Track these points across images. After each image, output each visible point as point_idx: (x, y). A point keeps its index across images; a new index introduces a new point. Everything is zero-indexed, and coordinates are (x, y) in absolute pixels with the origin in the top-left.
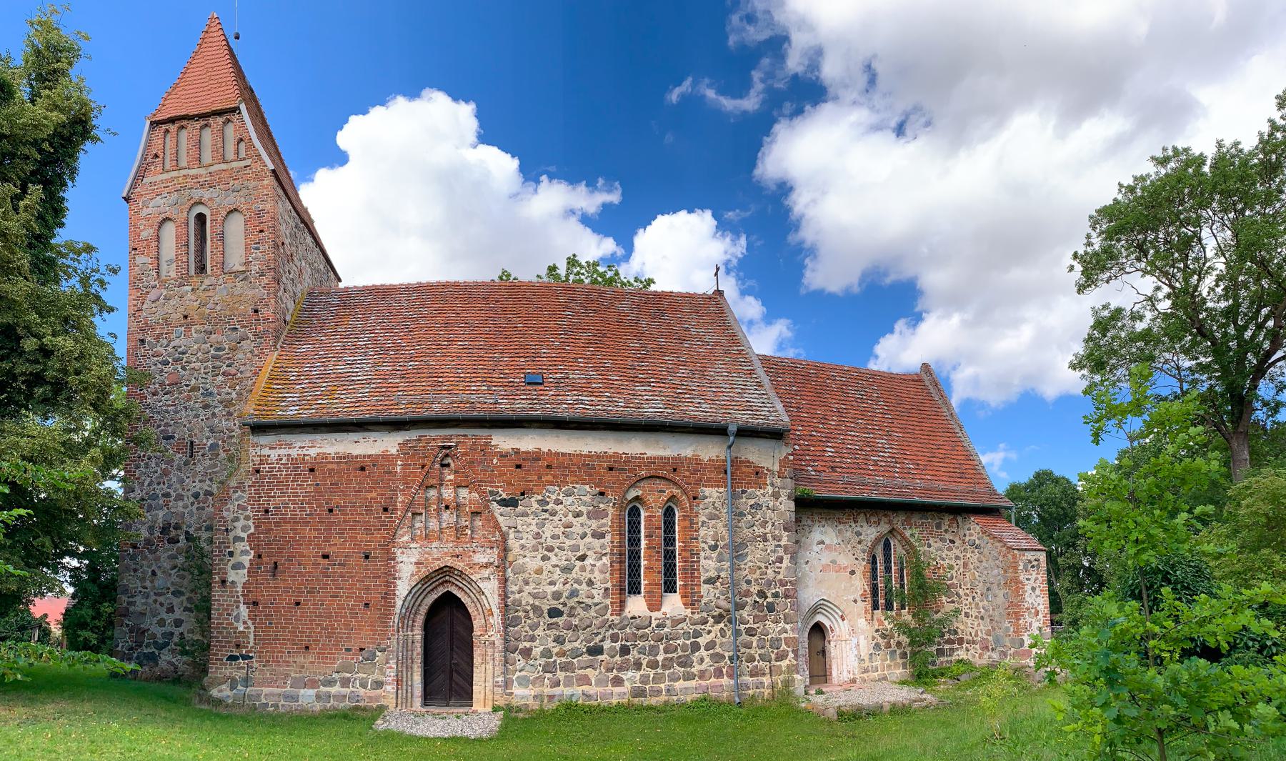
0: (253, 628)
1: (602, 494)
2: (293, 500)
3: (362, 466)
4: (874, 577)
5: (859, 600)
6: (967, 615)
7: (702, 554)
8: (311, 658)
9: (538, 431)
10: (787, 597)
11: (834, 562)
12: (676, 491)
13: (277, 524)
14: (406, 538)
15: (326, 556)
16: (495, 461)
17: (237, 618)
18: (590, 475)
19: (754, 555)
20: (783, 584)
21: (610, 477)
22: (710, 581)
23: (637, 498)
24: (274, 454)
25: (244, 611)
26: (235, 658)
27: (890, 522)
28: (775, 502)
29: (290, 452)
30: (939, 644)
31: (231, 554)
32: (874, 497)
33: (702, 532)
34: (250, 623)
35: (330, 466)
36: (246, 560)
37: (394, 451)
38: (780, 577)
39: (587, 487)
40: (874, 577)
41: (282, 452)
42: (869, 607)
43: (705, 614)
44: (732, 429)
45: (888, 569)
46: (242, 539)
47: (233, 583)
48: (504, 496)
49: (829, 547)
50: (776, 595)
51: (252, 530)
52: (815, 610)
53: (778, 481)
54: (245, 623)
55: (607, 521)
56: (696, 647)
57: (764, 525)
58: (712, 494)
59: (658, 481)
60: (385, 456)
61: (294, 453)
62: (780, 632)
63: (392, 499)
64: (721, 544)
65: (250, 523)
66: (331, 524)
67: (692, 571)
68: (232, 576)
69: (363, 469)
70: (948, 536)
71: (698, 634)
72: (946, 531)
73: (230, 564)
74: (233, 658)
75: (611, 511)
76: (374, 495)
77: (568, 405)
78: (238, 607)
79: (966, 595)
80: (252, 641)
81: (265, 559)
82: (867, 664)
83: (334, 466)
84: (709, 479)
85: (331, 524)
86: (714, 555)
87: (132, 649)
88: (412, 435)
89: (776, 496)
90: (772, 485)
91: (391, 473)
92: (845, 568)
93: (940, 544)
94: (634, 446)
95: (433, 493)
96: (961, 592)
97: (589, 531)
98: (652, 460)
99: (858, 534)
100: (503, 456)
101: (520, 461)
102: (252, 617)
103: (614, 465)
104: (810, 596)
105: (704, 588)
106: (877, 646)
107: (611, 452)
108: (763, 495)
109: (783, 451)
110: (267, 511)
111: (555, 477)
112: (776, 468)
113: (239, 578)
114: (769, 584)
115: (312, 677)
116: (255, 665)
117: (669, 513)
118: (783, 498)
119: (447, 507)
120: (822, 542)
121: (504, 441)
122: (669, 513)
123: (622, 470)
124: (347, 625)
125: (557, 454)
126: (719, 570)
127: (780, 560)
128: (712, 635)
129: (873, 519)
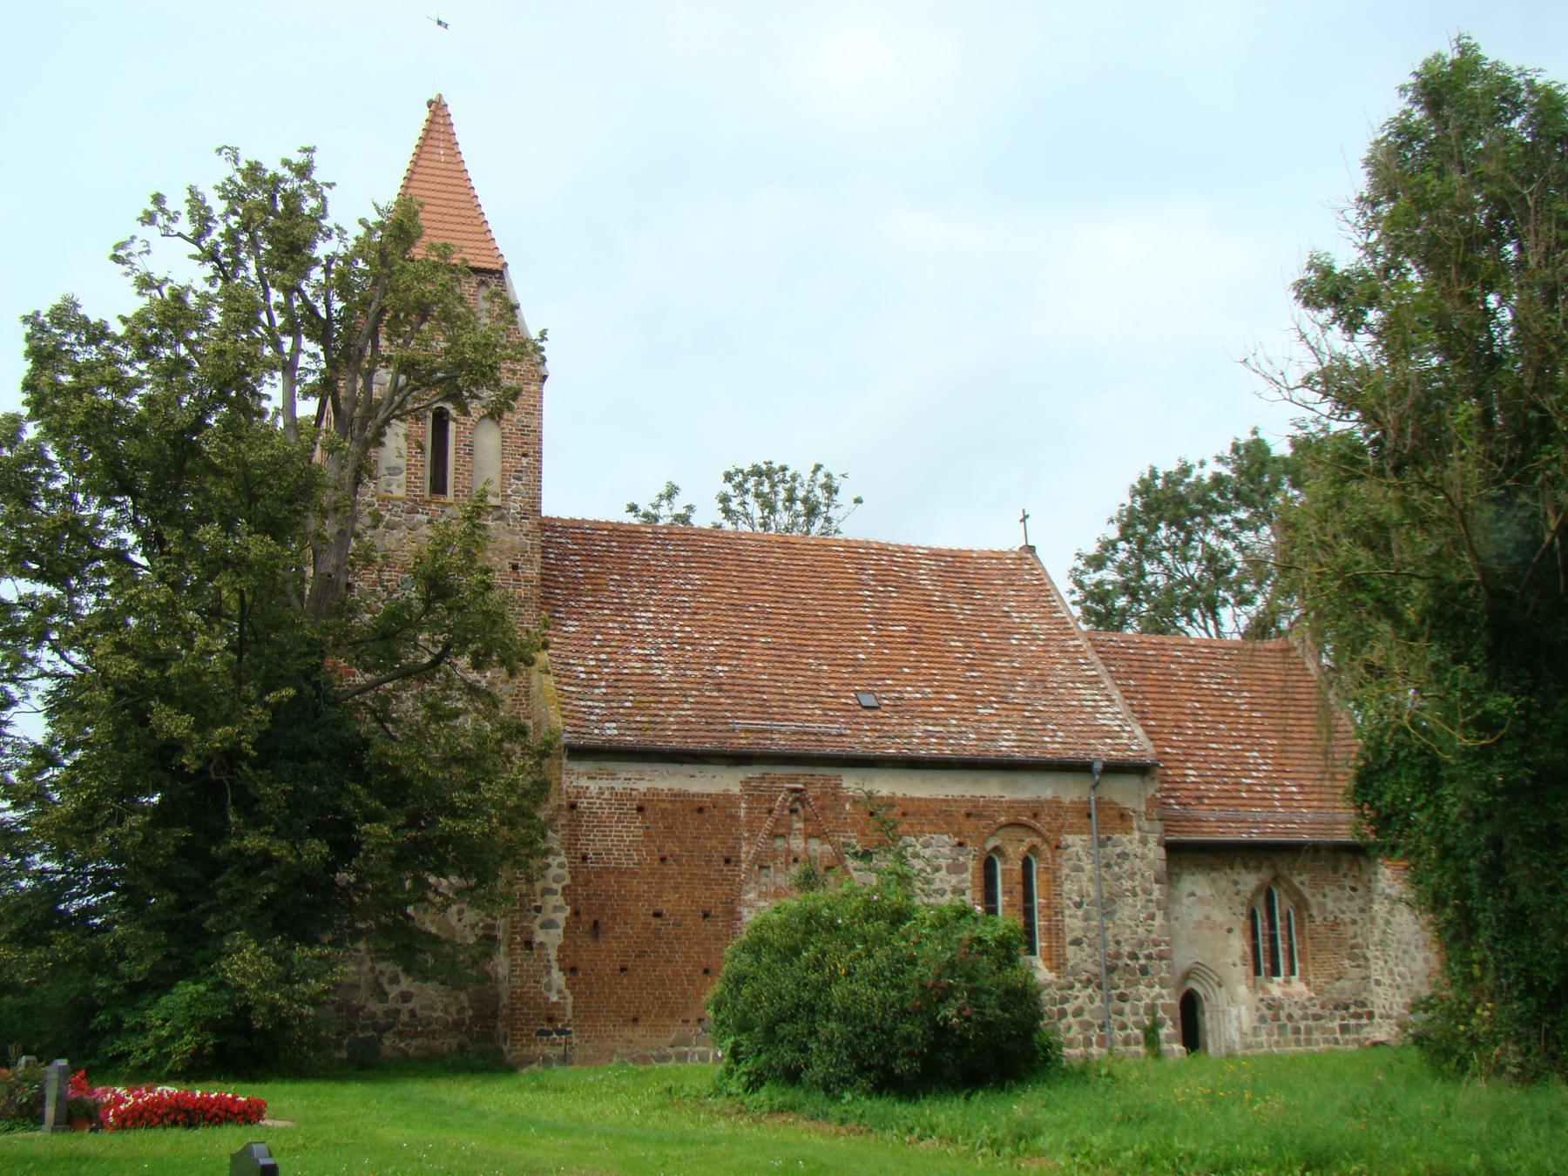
0: (570, 999)
1: (960, 844)
2: (620, 842)
3: (700, 807)
4: (1254, 935)
5: (1239, 962)
6: (1378, 983)
7: (1067, 912)
8: (640, 1031)
9: (891, 771)
10: (1161, 958)
11: (1207, 918)
12: (1036, 840)
13: (598, 875)
14: (752, 896)
15: (657, 915)
16: (848, 807)
17: (548, 987)
18: (948, 823)
19: (1126, 911)
20: (1156, 944)
21: (968, 826)
22: (1077, 942)
23: (996, 849)
24: (594, 787)
25: (558, 978)
26: (548, 1033)
27: (1274, 866)
28: (1143, 849)
29: (615, 784)
30: (1343, 1018)
31: (538, 909)
32: (1255, 838)
33: (1067, 886)
34: (567, 992)
35: (662, 805)
36: (561, 918)
37: (736, 789)
38: (1154, 936)
39: (945, 837)
40: (1254, 935)
41: (605, 784)
42: (1251, 971)
43: (1071, 979)
44: (1098, 766)
45: (1272, 926)
46: (554, 892)
47: (542, 945)
48: (858, 848)
49: (1201, 900)
50: (1149, 957)
51: (567, 881)
52: (1187, 976)
53: (1146, 825)
54: (559, 992)
55: (968, 876)
56: (1063, 1014)
57: (1132, 876)
58: (1076, 843)
59: (1016, 829)
60: (727, 797)
61: (619, 785)
62: (1155, 998)
63: (735, 849)
64: (1086, 900)
65: (565, 872)
66: (663, 877)
67: (1055, 932)
68: (540, 936)
69: (701, 810)
70: (1348, 882)
71: (1064, 1000)
72: (1345, 876)
73: (538, 921)
74: (542, 1033)
75: (971, 864)
76: (714, 842)
77: (920, 738)
78: (549, 973)
79: (1377, 958)
80: (569, 1015)
81: (584, 917)
82: (1250, 1039)
83: (668, 806)
84: (1071, 825)
85: (663, 877)
86: (1080, 913)
87: (340, 1033)
88: (753, 772)
89: (1144, 842)
90: (1140, 829)
91: (734, 818)
92: (1221, 925)
93: (1338, 893)
94: (991, 789)
95: (779, 843)
96: (1369, 955)
97: (948, 888)
98: (1012, 804)
99: (1236, 883)
100: (855, 802)
101: (874, 808)
102: (571, 985)
103: (975, 811)
104: (1184, 958)
105: (1071, 951)
106: (1262, 1019)
107: (968, 795)
108: (1129, 842)
109: (1152, 789)
110: (585, 858)
111: (911, 826)
112: (1143, 808)
113: (552, 940)
114: (1141, 944)
115: (642, 1052)
116: (575, 1040)
117: (1027, 864)
118: (1152, 845)
119: (796, 860)
120: (1193, 894)
121: (852, 783)
122: (1027, 864)
123: (980, 816)
124: (684, 993)
125: (912, 799)
126: (1086, 929)
127: (1152, 917)
128: (1080, 1001)
129: (1253, 864)
